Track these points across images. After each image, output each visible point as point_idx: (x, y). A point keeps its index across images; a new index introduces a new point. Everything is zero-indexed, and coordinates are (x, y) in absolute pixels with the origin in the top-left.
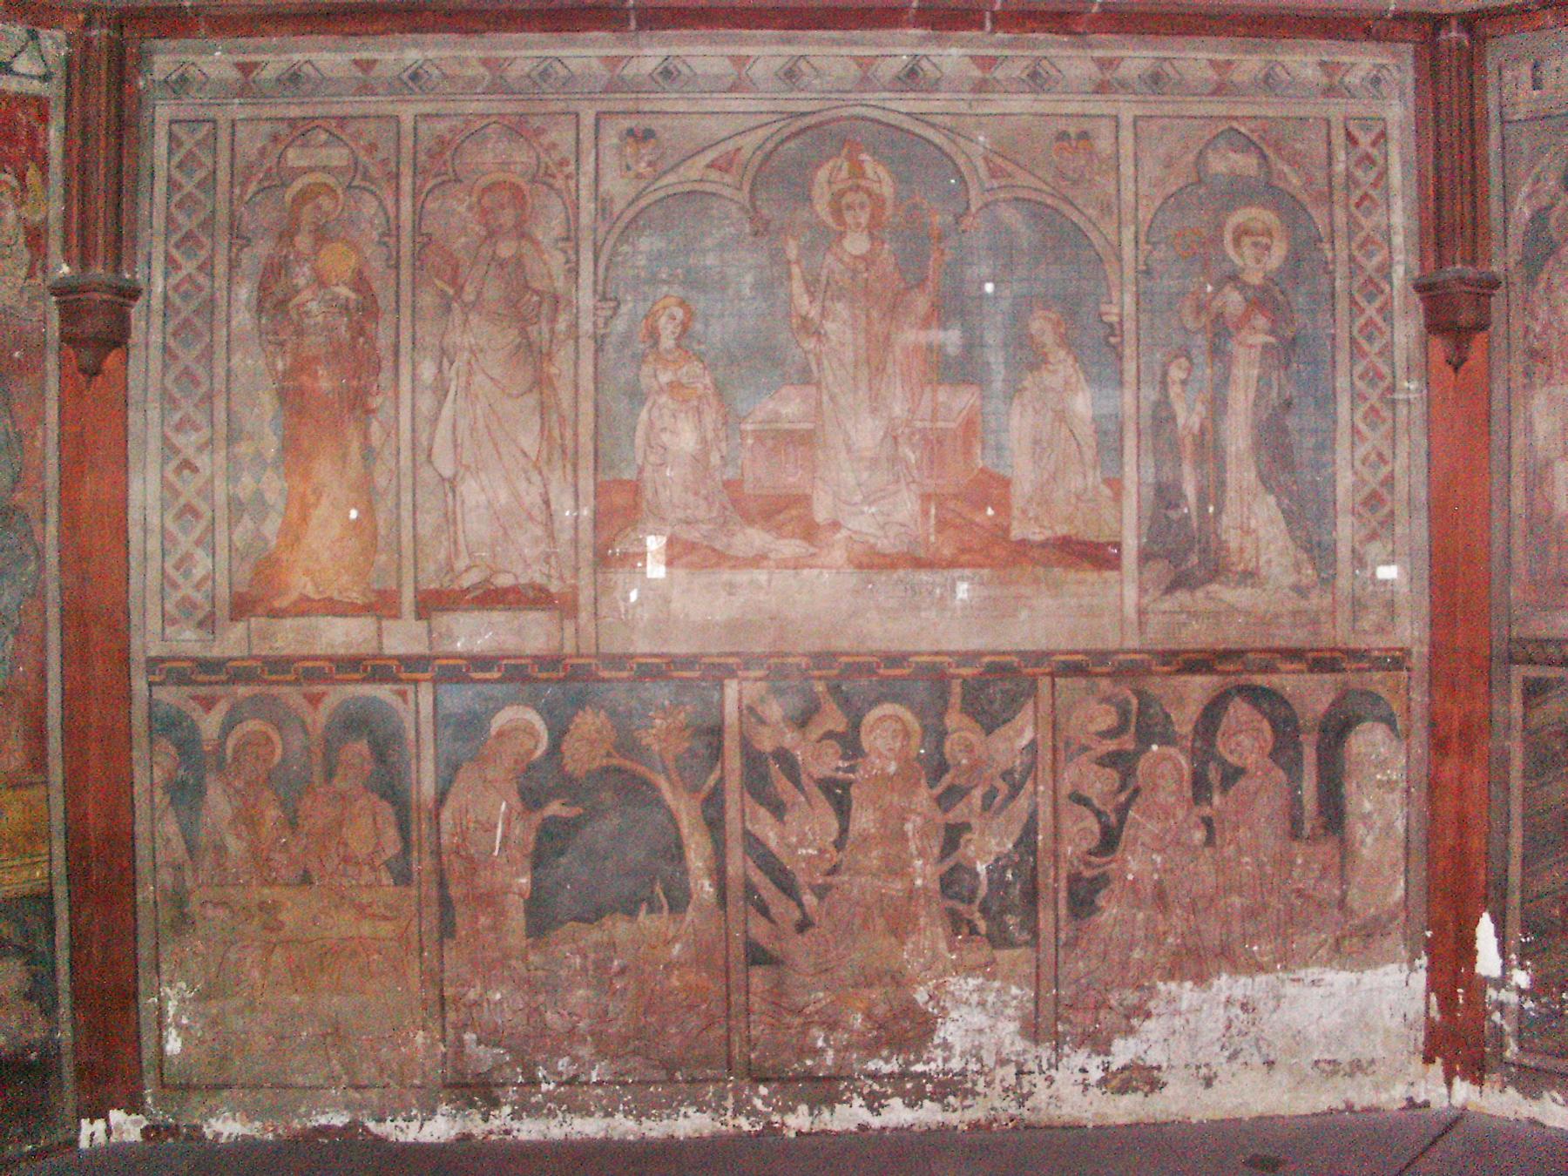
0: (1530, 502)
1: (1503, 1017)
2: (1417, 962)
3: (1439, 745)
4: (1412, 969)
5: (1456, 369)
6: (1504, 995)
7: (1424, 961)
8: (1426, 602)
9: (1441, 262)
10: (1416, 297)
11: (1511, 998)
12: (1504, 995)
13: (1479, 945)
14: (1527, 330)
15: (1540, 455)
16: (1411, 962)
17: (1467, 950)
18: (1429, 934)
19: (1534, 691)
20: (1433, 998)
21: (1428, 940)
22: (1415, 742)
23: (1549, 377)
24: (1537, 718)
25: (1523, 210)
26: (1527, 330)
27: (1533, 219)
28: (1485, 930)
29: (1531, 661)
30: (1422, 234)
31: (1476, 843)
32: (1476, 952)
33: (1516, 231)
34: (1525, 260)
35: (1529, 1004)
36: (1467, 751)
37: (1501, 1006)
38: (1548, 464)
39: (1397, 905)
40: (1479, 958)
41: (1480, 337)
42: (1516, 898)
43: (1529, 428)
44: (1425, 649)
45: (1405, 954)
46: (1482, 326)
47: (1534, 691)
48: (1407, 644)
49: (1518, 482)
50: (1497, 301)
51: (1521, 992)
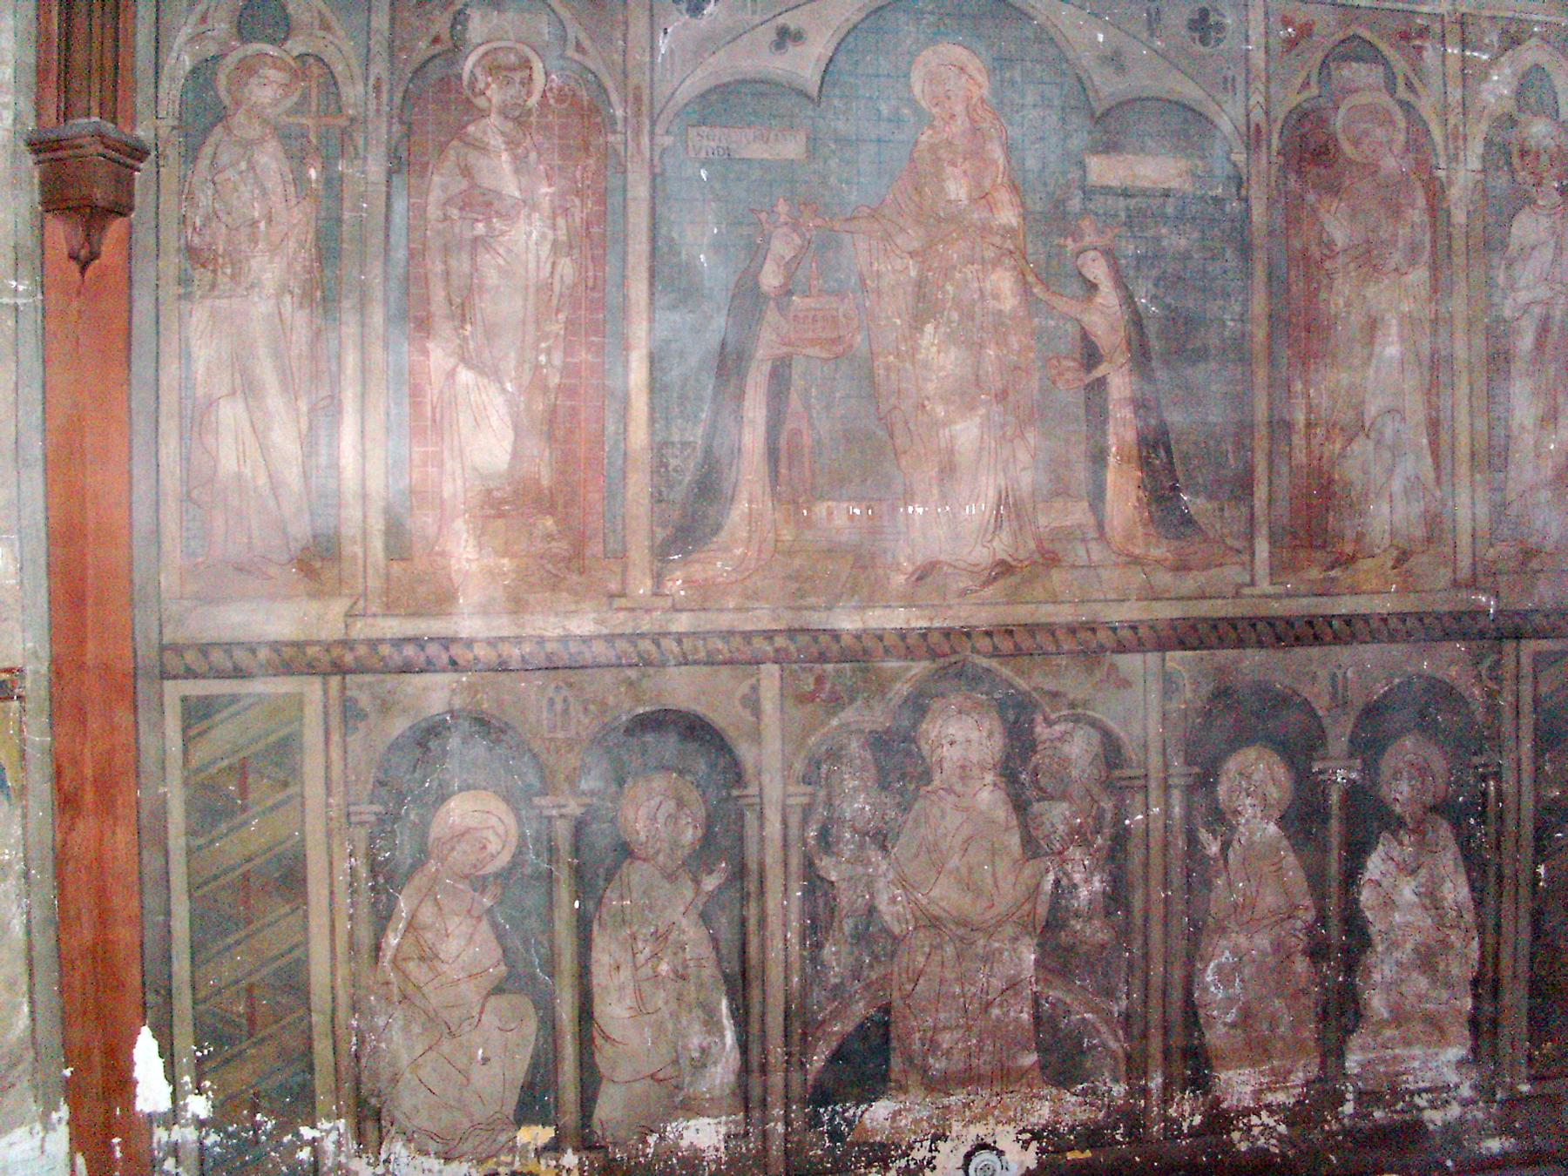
0: (186, 459)
1: (178, 1163)
2: (55, 1116)
3: (67, 803)
4: (48, 1127)
5: (83, 269)
6: (177, 1134)
7: (64, 1112)
8: (42, 598)
9: (66, 114)
10: (29, 160)
11: (186, 1134)
12: (177, 1134)
13: (138, 1073)
14: (183, 220)
15: (200, 392)
16: (45, 1117)
17: (122, 1083)
18: (67, 1072)
19: (198, 714)
20: (80, 1160)
21: (68, 1081)
22: (32, 802)
23: (213, 286)
24: (200, 755)
25: (180, 59)
26: (183, 220)
27: (194, 71)
28: (146, 1052)
29: (191, 674)
30: (41, 73)
31: (124, 934)
32: (135, 1083)
33: (171, 91)
34: (181, 127)
35: (213, 1138)
36: (106, 805)
37: (175, 1150)
38: (212, 403)
39: (21, 1041)
40: (139, 1090)
41: (116, 227)
42: (183, 1002)
43: (185, 356)
44: (44, 669)
45: (35, 1109)
46: (121, 209)
47: (198, 714)
48: (18, 662)
49: (169, 426)
50: (143, 175)
51: (200, 1124)
